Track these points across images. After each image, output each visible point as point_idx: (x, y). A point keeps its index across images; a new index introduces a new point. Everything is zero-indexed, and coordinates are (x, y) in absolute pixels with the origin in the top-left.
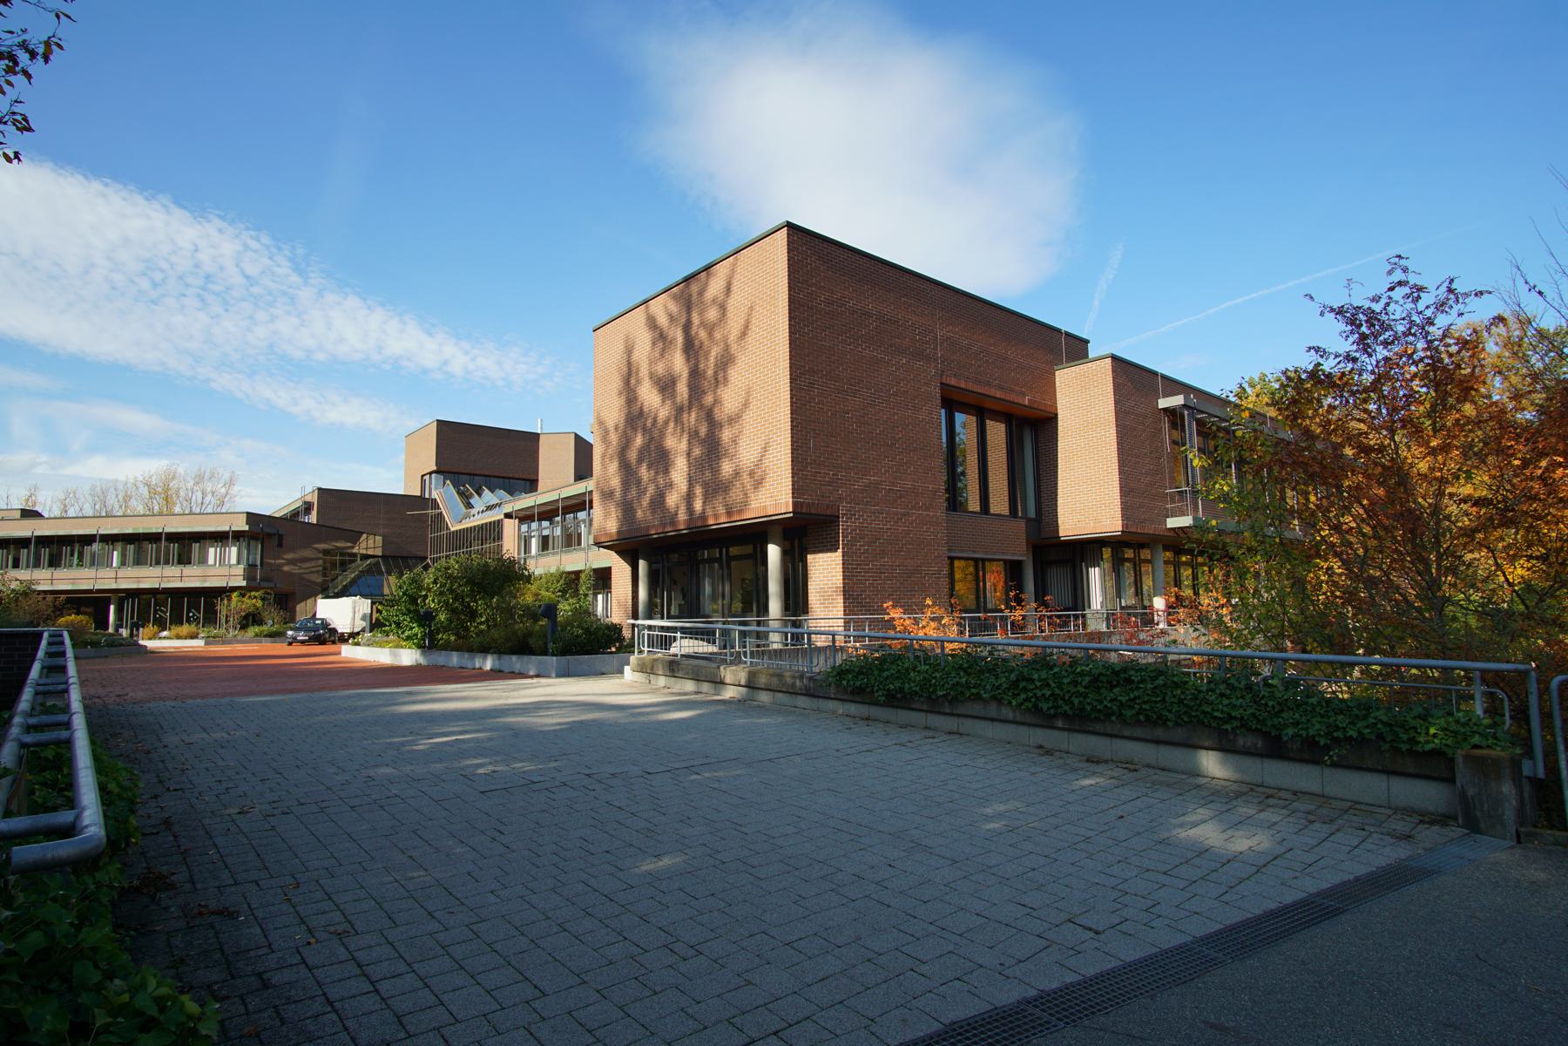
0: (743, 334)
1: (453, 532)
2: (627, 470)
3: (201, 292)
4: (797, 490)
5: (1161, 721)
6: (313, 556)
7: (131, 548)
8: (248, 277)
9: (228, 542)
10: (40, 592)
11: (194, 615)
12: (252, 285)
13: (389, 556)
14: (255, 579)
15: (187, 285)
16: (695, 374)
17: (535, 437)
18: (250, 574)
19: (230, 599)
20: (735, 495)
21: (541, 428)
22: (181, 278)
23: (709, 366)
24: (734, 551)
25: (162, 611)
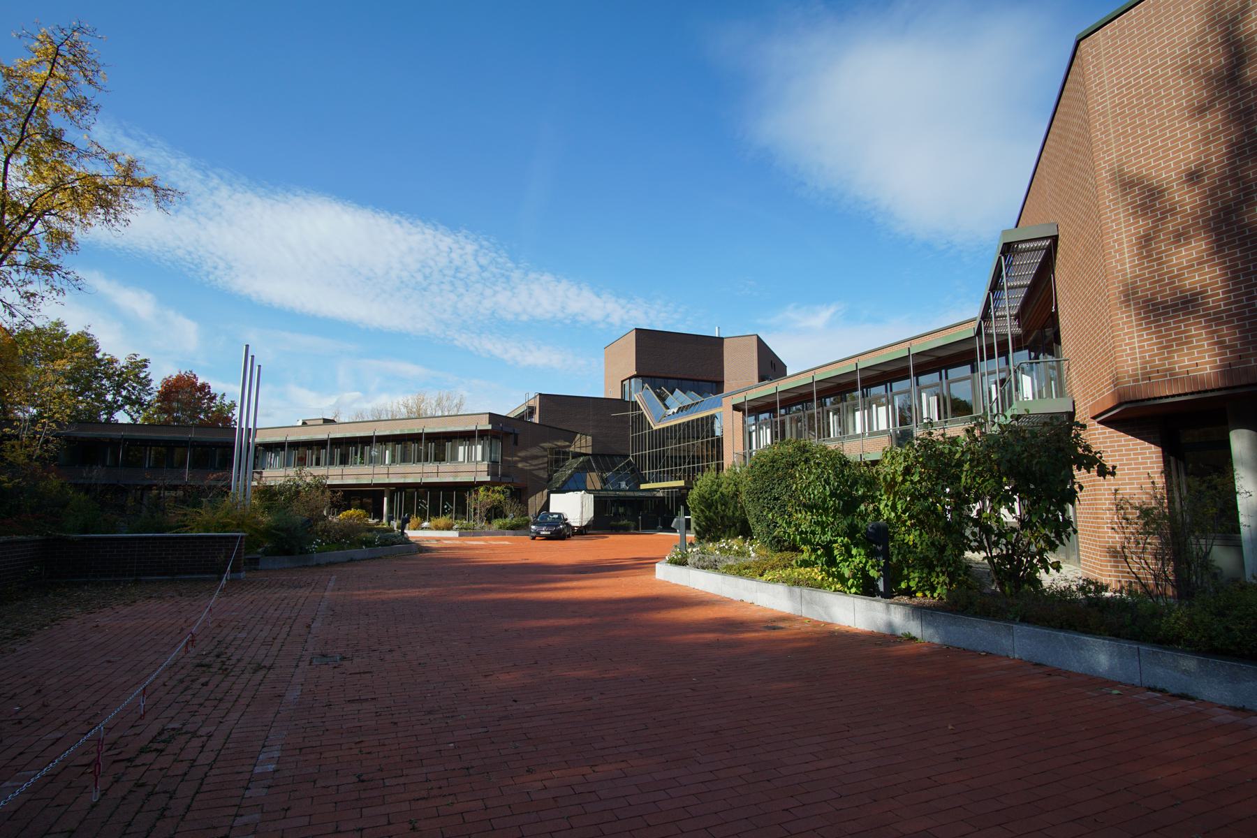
1: (656, 430)
3: (452, 279)
6: (540, 454)
7: (399, 447)
8: (481, 267)
9: (475, 440)
10: (330, 486)
11: (448, 507)
12: (483, 271)
13: (598, 455)
14: (497, 475)
15: (444, 275)
17: (719, 341)
18: (492, 471)
19: (476, 492)
22: (441, 271)
25: (422, 503)
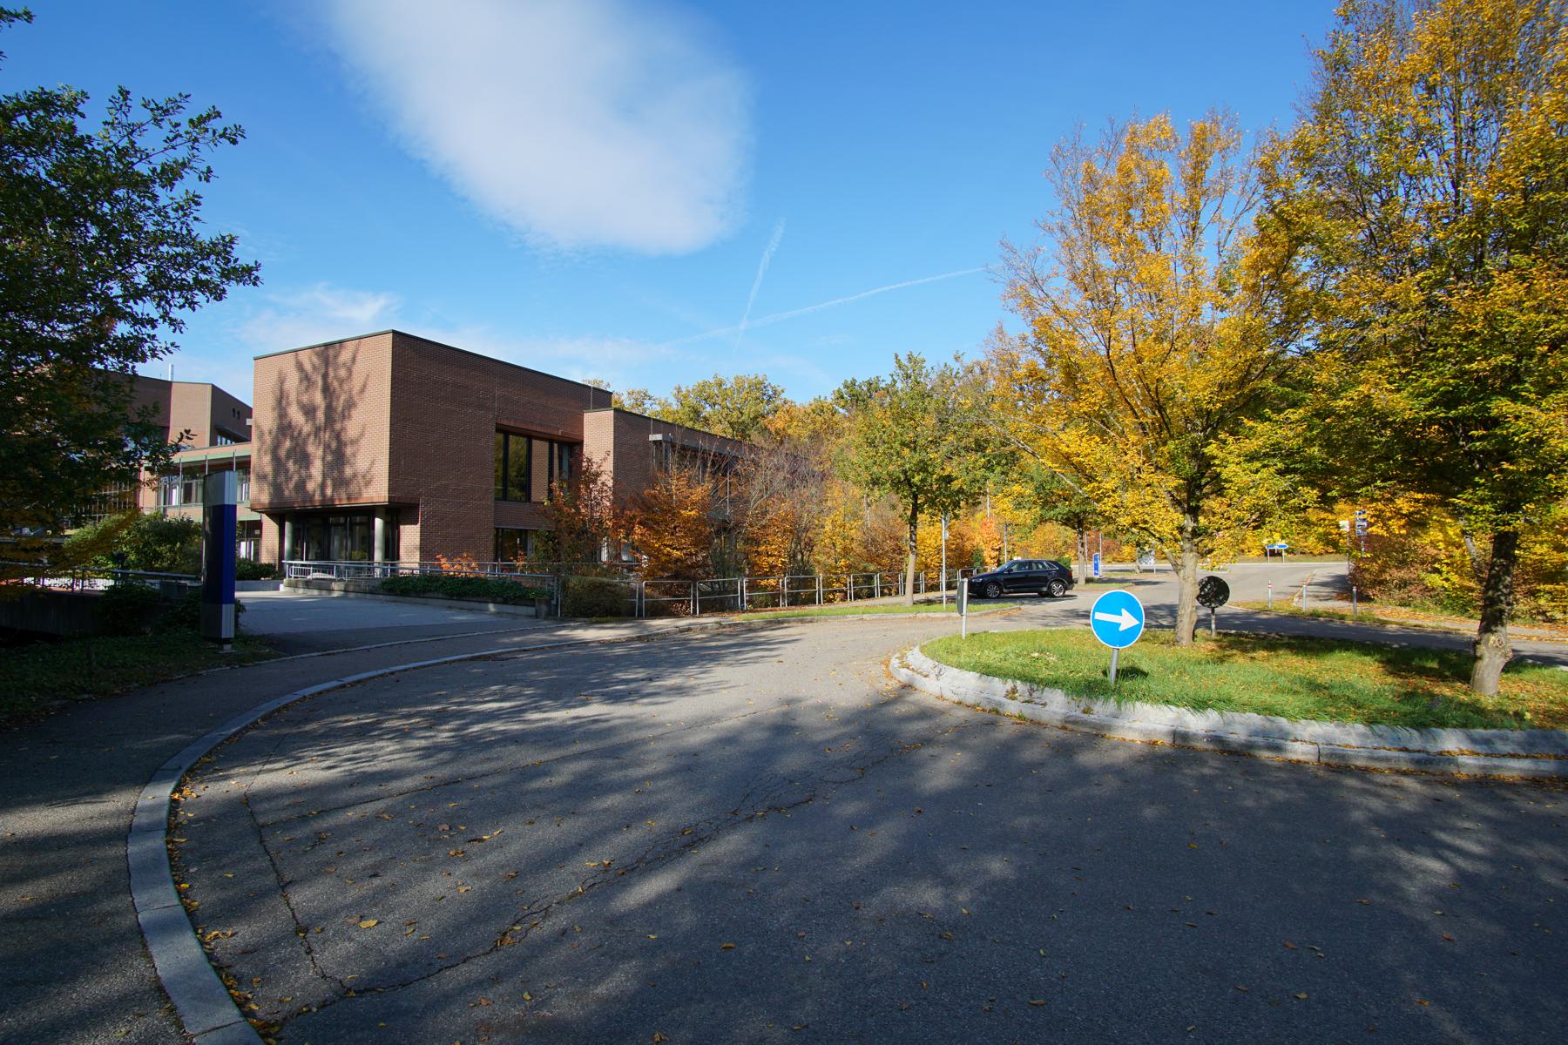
0: (362, 391)
2: (278, 463)
4: (391, 490)
5: (478, 595)
16: (329, 409)
20: (353, 488)
21: (172, 374)
23: (340, 404)
24: (358, 519)
